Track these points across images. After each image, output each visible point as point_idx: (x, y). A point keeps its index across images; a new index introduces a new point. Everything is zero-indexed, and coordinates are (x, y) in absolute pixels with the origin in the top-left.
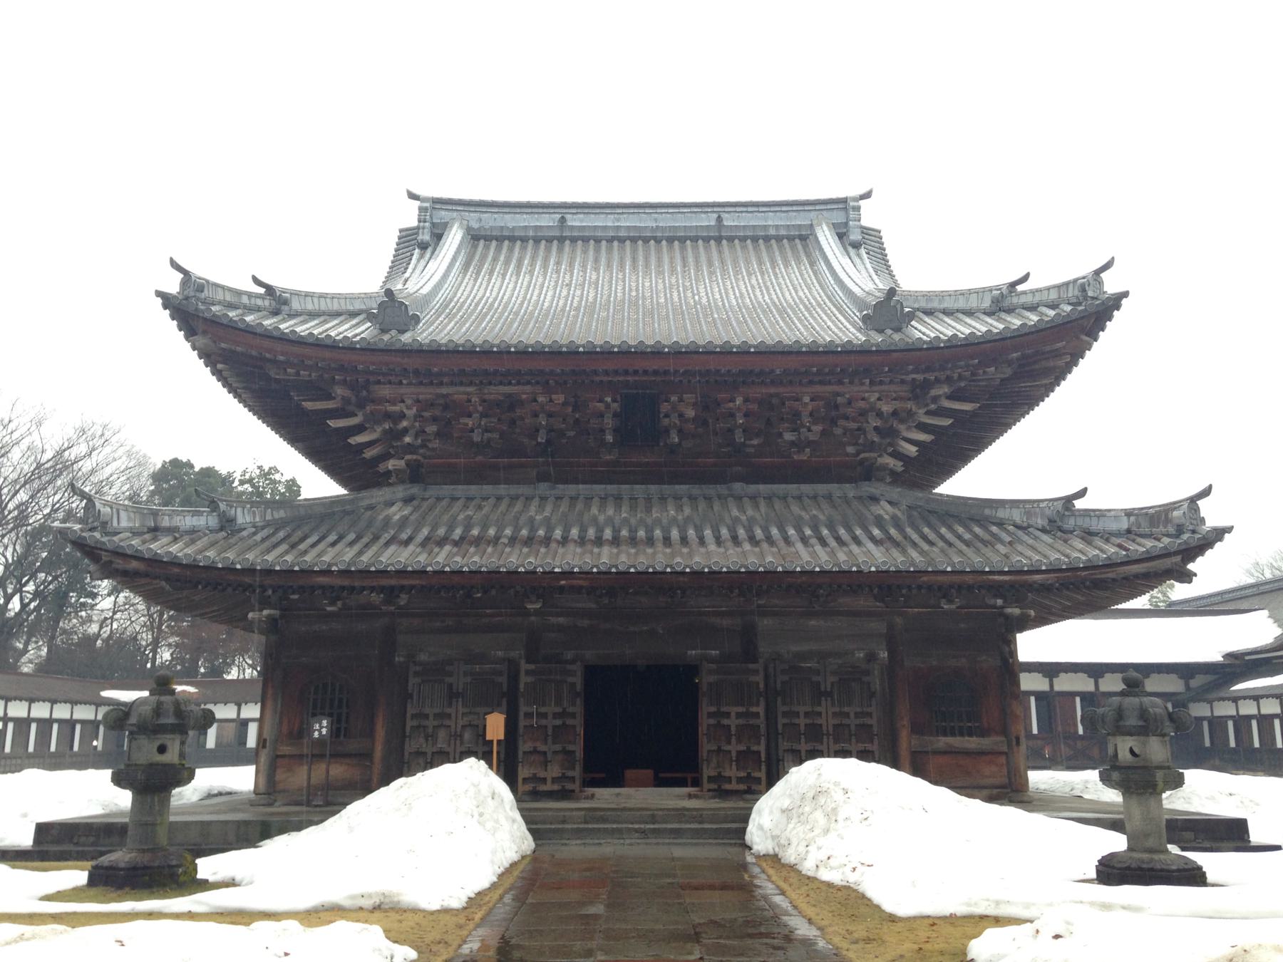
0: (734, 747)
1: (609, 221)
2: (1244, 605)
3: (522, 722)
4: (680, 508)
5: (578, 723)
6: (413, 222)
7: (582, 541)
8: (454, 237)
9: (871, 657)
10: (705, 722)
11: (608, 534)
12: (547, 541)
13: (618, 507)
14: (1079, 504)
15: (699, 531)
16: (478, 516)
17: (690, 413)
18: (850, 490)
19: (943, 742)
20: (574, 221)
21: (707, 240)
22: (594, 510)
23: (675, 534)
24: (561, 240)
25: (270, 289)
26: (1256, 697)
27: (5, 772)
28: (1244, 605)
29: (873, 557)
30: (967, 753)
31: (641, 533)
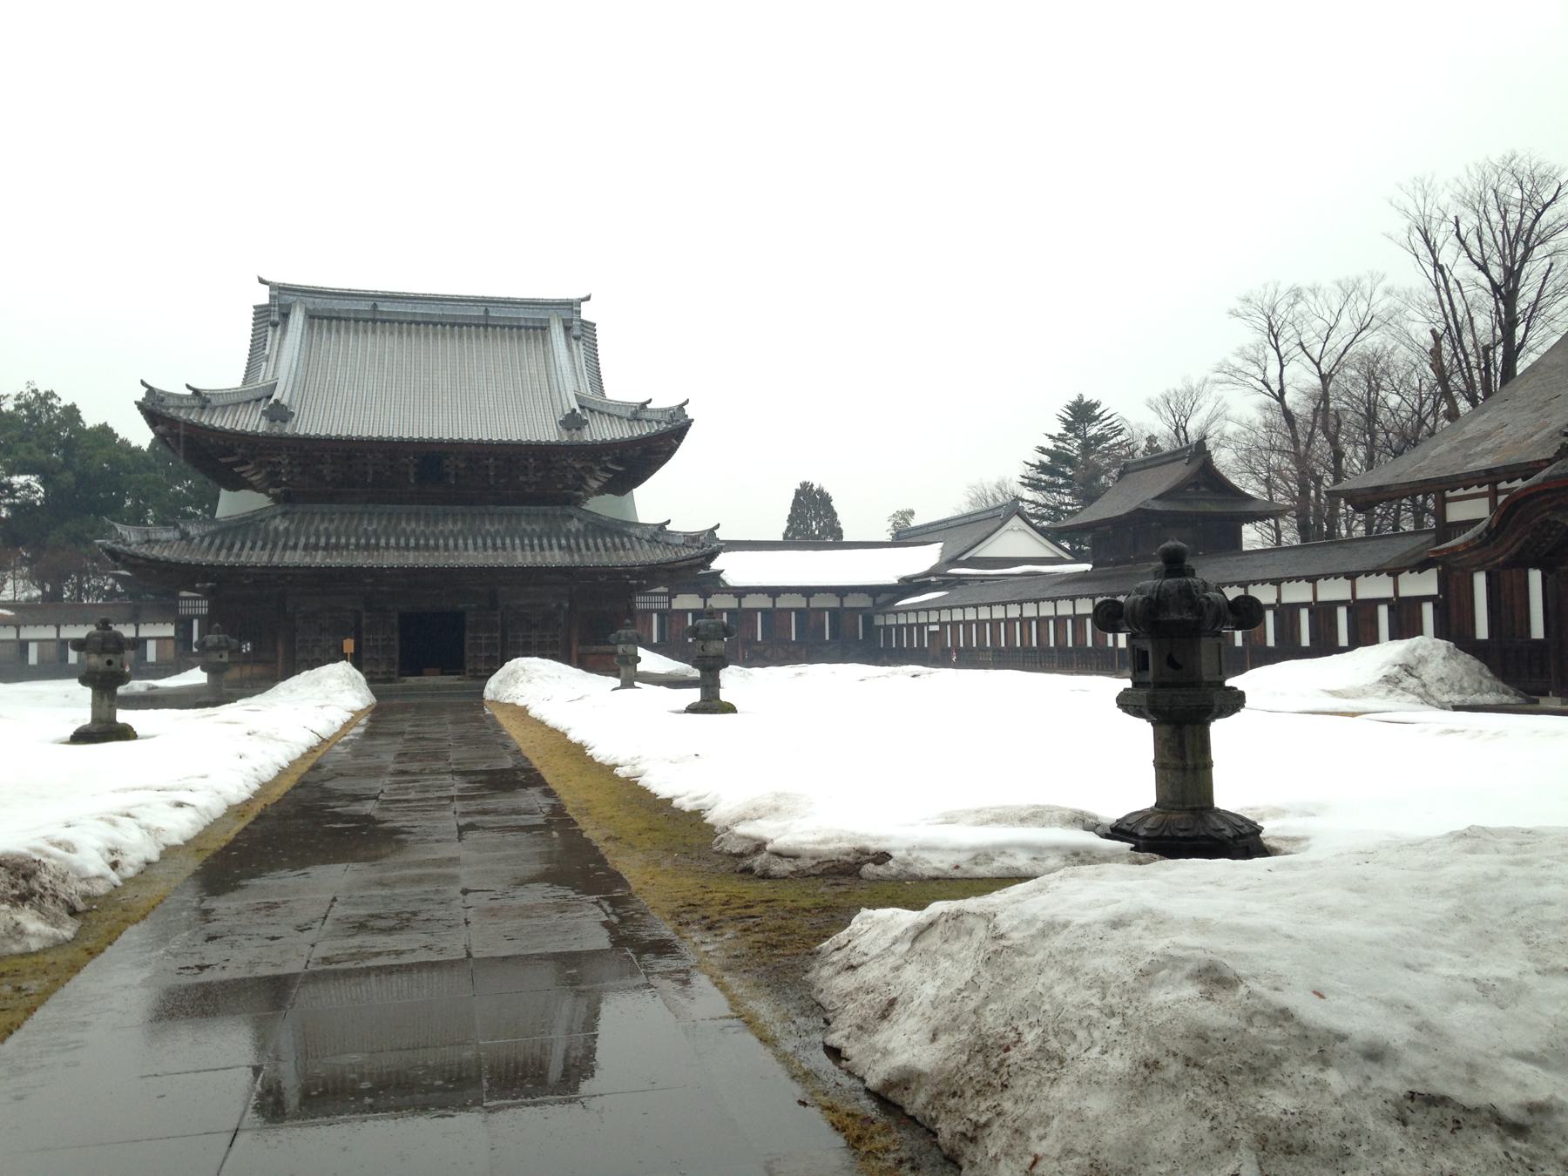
0: (484, 654)
1: (409, 308)
2: (926, 539)
3: (364, 643)
4: (455, 523)
5: (396, 643)
6: (266, 301)
7: (398, 547)
8: (297, 320)
9: (560, 607)
10: (468, 642)
11: (412, 542)
12: (377, 547)
13: (418, 521)
14: (668, 527)
15: (465, 540)
16: (332, 527)
17: (463, 465)
18: (558, 510)
19: (595, 649)
20: (384, 307)
21: (477, 326)
22: (403, 524)
23: (451, 542)
24: (374, 321)
25: (196, 392)
26: (916, 609)
27: (6, 681)
28: (926, 539)
29: (556, 557)
30: (603, 654)
31: (432, 542)
